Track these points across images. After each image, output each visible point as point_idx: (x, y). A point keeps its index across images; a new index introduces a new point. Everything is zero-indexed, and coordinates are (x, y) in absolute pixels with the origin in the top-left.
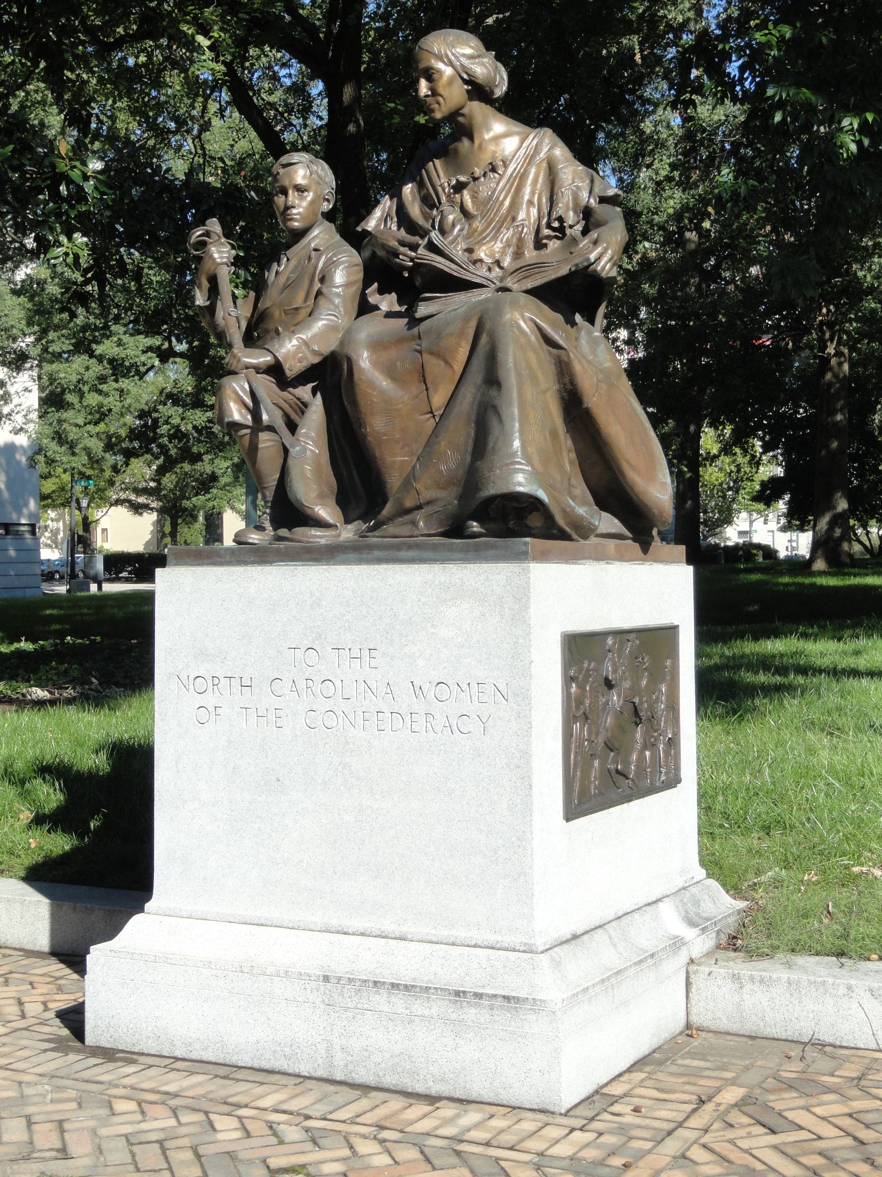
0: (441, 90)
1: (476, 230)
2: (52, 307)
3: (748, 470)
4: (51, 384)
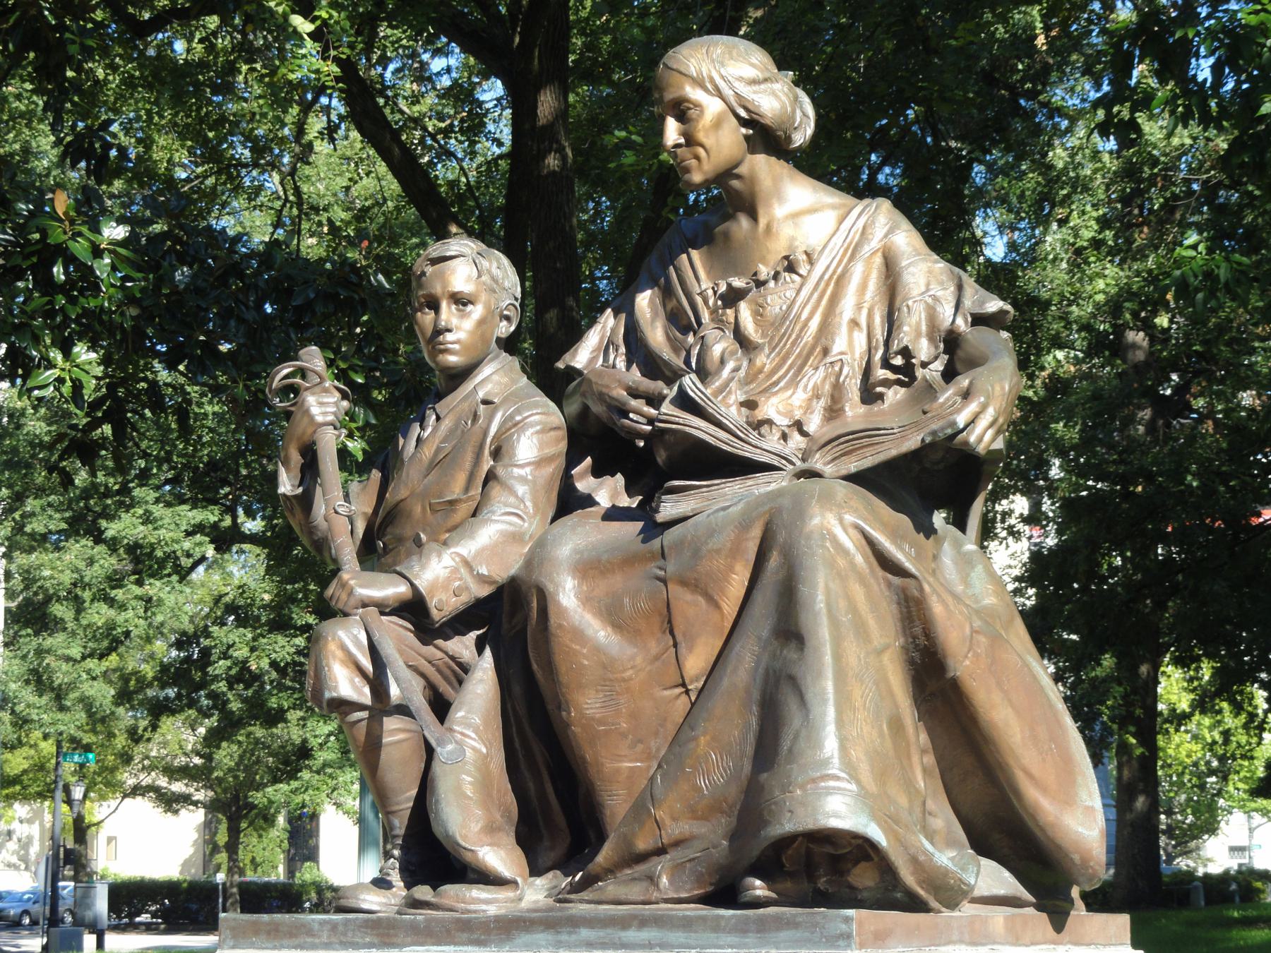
0: (701, 136)
1: (760, 371)
2: (33, 456)
3: (1243, 739)
4: (27, 588)
